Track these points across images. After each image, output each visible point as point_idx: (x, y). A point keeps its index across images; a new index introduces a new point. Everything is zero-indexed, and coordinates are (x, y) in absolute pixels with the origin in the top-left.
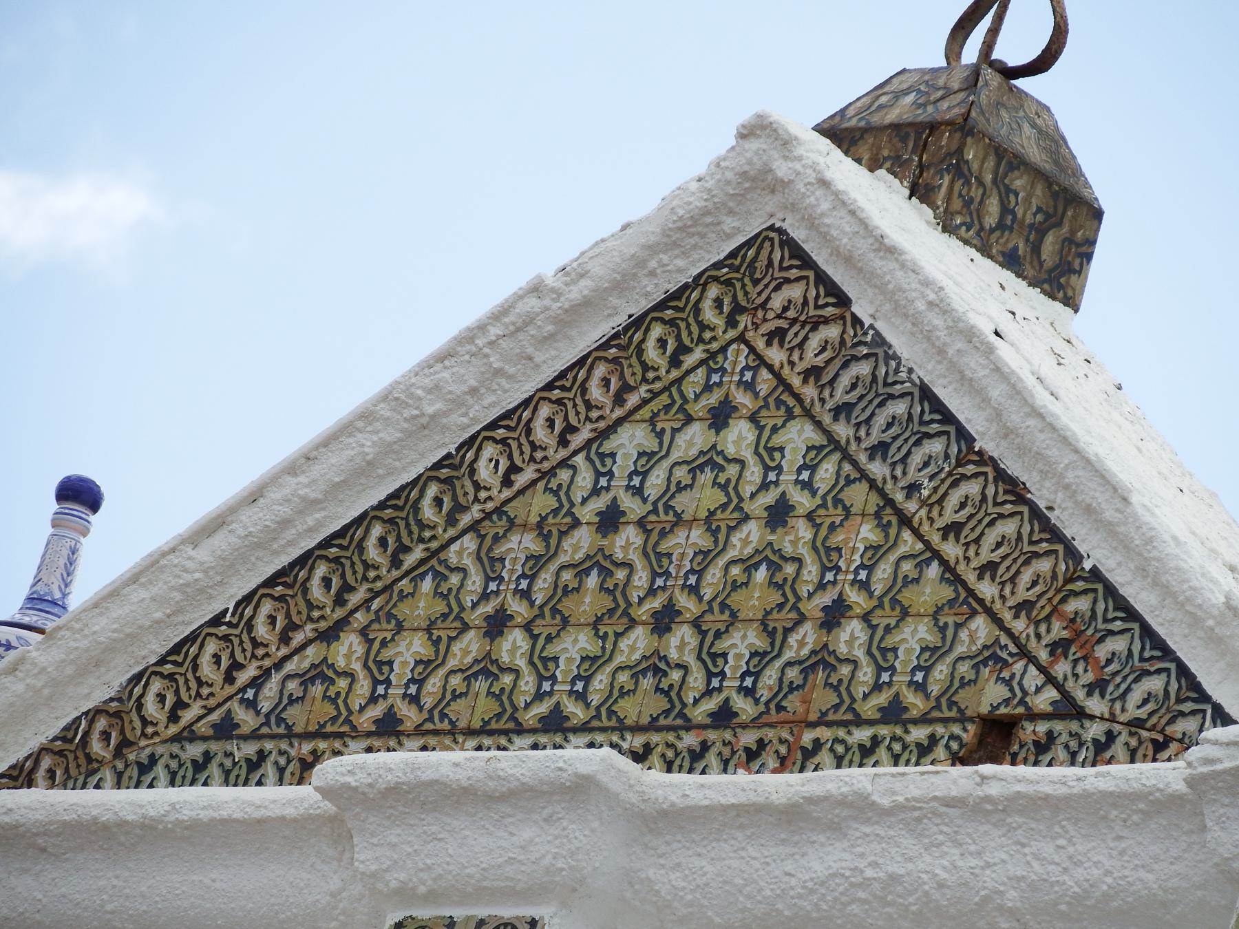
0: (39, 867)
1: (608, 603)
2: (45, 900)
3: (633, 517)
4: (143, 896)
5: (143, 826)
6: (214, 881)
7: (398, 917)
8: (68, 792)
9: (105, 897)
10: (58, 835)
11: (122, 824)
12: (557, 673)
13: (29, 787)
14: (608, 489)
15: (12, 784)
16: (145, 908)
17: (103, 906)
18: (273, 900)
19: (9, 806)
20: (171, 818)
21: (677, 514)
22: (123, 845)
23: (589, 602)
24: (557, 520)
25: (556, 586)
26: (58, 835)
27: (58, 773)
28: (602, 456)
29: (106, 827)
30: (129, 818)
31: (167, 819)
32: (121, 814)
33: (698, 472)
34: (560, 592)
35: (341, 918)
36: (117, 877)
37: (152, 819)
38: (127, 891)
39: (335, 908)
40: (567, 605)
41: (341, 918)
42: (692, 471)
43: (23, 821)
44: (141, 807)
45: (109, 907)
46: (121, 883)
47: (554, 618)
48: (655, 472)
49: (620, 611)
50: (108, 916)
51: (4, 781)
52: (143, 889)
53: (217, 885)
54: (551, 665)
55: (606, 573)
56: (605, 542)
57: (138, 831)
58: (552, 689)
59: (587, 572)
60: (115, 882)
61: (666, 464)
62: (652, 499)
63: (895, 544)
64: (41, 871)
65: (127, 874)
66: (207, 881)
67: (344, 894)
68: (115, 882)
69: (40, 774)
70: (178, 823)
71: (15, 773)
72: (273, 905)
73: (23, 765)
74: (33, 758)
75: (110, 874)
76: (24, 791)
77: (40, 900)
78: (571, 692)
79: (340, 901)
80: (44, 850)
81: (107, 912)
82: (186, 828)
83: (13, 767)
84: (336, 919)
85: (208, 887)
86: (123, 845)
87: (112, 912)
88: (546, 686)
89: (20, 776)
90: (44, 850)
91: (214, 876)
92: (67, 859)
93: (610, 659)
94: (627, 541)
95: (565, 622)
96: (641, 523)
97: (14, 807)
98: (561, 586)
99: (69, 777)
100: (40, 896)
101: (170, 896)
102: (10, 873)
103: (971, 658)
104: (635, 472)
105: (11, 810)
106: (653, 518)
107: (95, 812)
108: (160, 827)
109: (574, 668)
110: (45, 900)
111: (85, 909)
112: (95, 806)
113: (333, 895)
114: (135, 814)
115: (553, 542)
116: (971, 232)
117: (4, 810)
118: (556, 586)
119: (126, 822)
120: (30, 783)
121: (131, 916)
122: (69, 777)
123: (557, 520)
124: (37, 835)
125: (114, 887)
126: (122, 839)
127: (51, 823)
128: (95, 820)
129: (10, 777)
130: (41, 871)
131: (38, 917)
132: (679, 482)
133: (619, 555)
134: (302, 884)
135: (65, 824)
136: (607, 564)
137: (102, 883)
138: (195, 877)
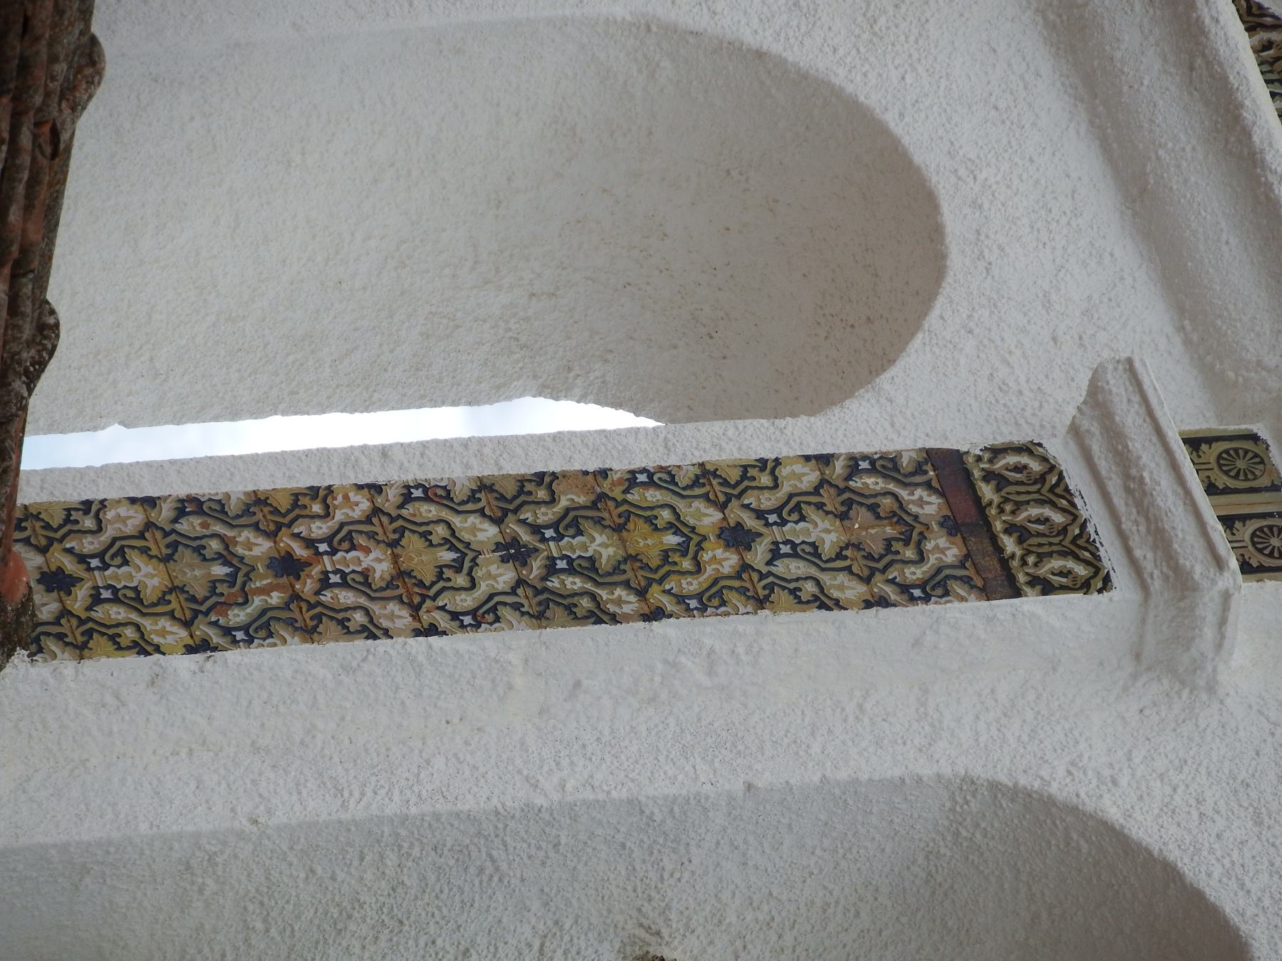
0: (1173, 70)
1: (200, 592)
2: (1143, 89)
3: (749, 557)
4: (1186, 181)
5: (1253, 154)
6: (1227, 243)
7: (1263, 434)
8: (1257, 70)
9: (1170, 145)
10: (1212, 76)
11: (1246, 134)
12: (340, 554)
13: (1246, 30)
14: (767, 524)
15: (1243, 11)
16: (1175, 187)
17: (1160, 146)
18: (1231, 307)
19: (1221, 19)
20: (1271, 178)
21: (767, 597)
22: (1227, 142)
23: (194, 575)
24: (717, 488)
25: (427, 524)
26: (1212, 76)
27: (1271, 52)
28: (798, 508)
29: (1237, 119)
30: (1256, 138)
31: (1268, 173)
32: (1255, 128)
33: (593, 620)
34: (195, 544)
35: (1240, 379)
36: (1194, 149)
37: (1263, 160)
38: (1184, 164)
39: (1247, 370)
40: (185, 555)
41: (1240, 379)
42: (816, 598)
43: (1212, 36)
44: (1271, 144)
45: (1161, 152)
46: (1189, 155)
47: (394, 531)
48: (801, 564)
49: (425, 592)
50: (1153, 156)
51: (1244, 4)
52: (1193, 179)
53: (1225, 248)
54: (118, 560)
55: (683, 550)
56: (935, 527)
57: (1246, 152)
58: (93, 569)
59: (452, 548)
60: (1188, 149)
61: (813, 571)
62: (773, 569)
63: (459, 512)
64: (1171, 74)
65: (1201, 157)
66: (1224, 237)
67: (1264, 373)
68: (1188, 149)
69: (1264, 36)
70: (1269, 186)
71: (1254, 10)
72: (1226, 309)
73: (1265, 16)
74: (1276, 22)
75: (1194, 142)
76: (1241, 27)
77: (1142, 84)
78: (96, 588)
79: (1256, 372)
80: (1192, 69)
81: (1156, 154)
82: (1267, 197)
83: (1260, 7)
84: (1237, 375)
85: (1219, 240)
86: (1227, 142)
87: (1158, 158)
88: (95, 563)
89: (1254, 18)
90: (1192, 69)
91: (1231, 241)
92: (1191, 94)
93: (144, 615)
94: (722, 560)
95: (393, 544)
96: (745, 567)
97: (1222, 23)
98: (655, 512)
99: (1272, 64)
100: (1146, 82)
101: (1195, 206)
102: (1157, 45)
103: (371, 621)
104: (794, 546)
105: (1217, 21)
106: (755, 577)
107: (1247, 102)
108: (1259, 170)
109: (123, 583)
110: (1143, 89)
111: (1151, 131)
112: (1254, 101)
113: (1259, 363)
114: (1262, 143)
115: (470, 507)
116: (244, 822)
117: (1215, 15)
118: (427, 524)
119: (1250, 136)
120: (1250, 29)
121: (1162, 178)
122: (1272, 64)
123: (717, 488)
124: (1204, 55)
125: (1183, 149)
126: (1233, 139)
127: (1220, 64)
128: (1240, 106)
129: (1249, 8)
130: (1171, 74)
131: (1125, 89)
132: (800, 590)
133: (479, 573)
134: (1257, 328)
135: (1225, 79)
136: (467, 564)
137: (1183, 137)
138: (1223, 223)
